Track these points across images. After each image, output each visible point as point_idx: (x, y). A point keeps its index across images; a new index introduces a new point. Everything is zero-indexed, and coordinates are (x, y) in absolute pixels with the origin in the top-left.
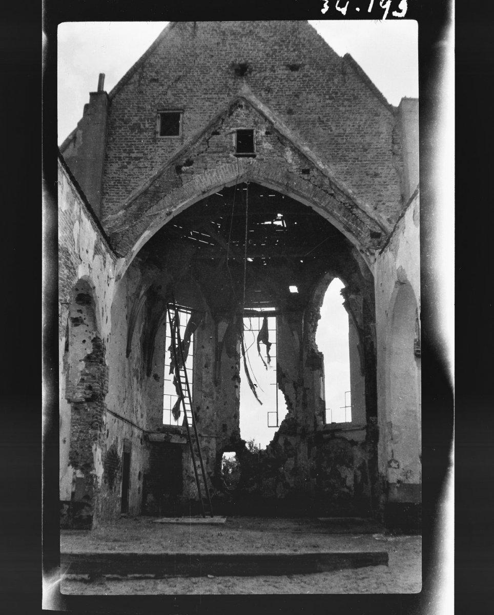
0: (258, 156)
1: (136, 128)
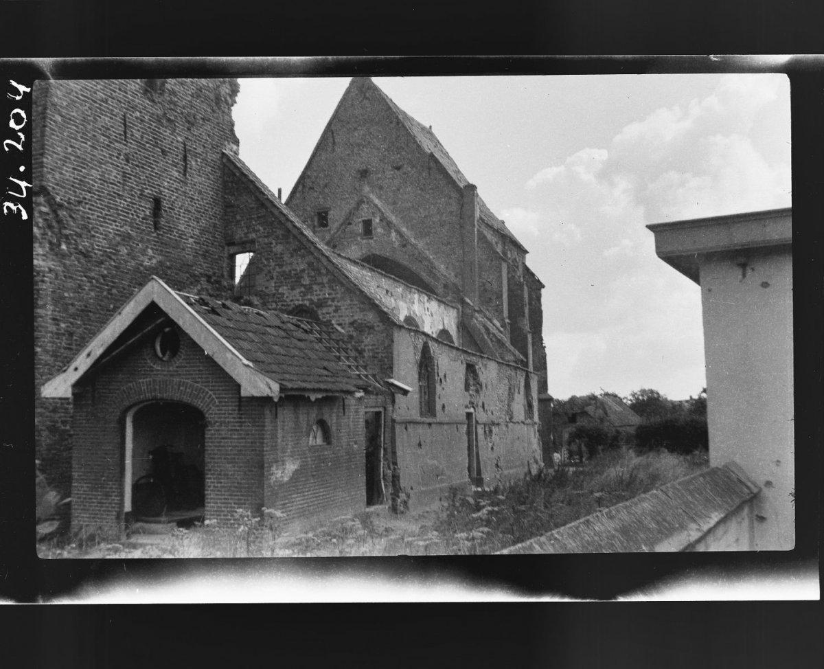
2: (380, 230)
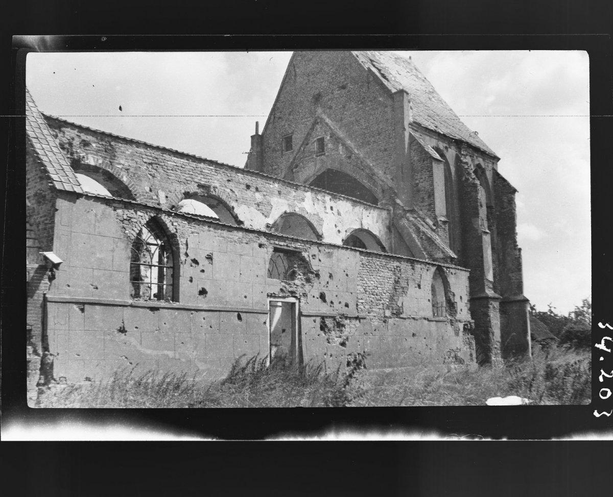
0: (327, 154)
1: (274, 150)
2: (330, 146)
